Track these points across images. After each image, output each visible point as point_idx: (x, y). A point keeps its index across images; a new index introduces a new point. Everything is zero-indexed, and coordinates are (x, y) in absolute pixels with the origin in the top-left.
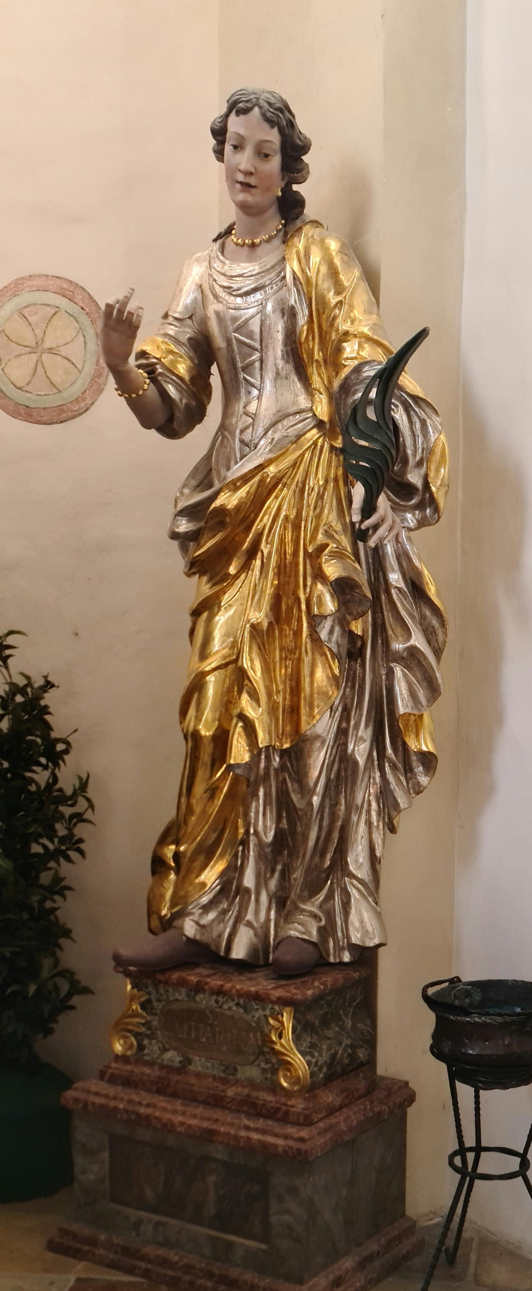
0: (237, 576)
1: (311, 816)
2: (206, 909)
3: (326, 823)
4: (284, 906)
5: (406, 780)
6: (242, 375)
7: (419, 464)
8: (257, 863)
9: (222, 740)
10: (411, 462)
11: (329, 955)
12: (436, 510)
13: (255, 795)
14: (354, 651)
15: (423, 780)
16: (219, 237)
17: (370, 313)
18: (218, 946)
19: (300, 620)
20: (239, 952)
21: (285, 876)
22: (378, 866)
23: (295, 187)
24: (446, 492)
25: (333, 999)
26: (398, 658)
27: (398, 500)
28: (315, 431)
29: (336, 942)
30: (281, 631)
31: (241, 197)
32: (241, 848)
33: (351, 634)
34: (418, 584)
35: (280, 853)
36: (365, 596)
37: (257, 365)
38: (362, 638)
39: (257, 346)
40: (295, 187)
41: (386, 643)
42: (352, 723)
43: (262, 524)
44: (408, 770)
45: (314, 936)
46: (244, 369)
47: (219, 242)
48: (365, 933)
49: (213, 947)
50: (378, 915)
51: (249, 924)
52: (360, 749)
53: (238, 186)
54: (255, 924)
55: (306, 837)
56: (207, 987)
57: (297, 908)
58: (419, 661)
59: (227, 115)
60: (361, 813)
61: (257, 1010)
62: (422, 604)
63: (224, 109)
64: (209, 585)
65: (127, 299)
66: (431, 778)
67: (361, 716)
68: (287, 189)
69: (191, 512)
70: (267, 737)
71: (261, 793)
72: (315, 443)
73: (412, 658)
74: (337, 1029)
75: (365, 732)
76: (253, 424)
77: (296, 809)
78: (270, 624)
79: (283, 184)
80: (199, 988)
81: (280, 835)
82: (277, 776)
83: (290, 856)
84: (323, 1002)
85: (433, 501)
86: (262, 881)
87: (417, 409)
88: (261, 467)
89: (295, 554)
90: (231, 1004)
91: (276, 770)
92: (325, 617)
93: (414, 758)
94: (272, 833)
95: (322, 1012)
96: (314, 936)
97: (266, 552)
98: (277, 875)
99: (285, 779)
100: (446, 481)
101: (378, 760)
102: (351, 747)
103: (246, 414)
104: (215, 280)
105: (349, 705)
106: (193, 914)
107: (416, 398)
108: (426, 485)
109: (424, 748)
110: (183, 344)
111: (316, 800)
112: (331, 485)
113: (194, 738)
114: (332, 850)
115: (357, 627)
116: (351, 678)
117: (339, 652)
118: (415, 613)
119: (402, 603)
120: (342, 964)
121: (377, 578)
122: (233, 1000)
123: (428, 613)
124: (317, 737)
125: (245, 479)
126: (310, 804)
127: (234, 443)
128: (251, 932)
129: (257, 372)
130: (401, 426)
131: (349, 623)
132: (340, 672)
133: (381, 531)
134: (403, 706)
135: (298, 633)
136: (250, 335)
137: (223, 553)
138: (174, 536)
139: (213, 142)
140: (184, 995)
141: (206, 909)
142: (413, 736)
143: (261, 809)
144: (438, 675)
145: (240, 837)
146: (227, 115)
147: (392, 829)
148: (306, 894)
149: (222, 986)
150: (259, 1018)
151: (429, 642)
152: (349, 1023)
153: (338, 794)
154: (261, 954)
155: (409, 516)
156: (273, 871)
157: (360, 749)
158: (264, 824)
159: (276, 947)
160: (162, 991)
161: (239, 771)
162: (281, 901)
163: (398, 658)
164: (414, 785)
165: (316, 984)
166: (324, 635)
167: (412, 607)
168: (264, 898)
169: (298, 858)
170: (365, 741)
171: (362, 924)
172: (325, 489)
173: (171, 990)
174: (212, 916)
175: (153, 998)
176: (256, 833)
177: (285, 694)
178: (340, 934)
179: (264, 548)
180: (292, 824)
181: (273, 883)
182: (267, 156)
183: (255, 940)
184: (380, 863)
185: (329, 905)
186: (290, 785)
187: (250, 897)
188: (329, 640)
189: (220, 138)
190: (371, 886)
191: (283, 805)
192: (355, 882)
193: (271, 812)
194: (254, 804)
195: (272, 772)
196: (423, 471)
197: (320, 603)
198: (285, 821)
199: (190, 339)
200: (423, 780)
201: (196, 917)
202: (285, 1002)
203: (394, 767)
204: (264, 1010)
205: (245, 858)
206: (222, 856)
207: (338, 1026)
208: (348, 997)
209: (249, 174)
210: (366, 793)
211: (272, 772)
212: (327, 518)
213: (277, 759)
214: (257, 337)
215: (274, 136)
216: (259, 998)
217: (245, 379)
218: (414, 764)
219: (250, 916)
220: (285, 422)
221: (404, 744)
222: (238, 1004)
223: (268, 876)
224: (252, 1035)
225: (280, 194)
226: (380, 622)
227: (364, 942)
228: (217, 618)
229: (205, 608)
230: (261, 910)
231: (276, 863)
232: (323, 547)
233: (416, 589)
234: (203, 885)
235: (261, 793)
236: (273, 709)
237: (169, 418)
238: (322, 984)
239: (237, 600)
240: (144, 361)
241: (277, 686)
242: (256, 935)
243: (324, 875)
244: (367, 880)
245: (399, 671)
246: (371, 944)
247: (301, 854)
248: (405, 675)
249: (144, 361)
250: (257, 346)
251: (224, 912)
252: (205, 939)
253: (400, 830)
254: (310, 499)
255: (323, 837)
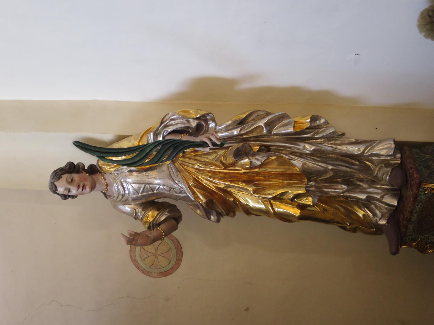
0: (235, 198)
1: (336, 170)
2: (375, 215)
3: (340, 163)
4: (375, 181)
5: (322, 128)
6: (155, 192)
7: (188, 121)
8: (355, 193)
9: (302, 207)
10: (187, 125)
11: (397, 163)
12: (208, 114)
13: (326, 193)
14: (267, 149)
15: (322, 121)
16: (106, 197)
17: (130, 140)
18: (391, 210)
19: (253, 172)
20: (395, 203)
21: (361, 180)
22: (359, 141)
23: (86, 168)
24: (200, 110)
25: (417, 163)
26: (269, 131)
27: (203, 131)
28: (176, 164)
29: (391, 160)
30: (257, 181)
31: (88, 189)
32: (349, 199)
33: (259, 151)
34: (238, 122)
35: (352, 182)
36: (242, 145)
37: (151, 186)
38: (261, 146)
39: (144, 185)
40: (86, 168)
41: (264, 136)
42: (297, 151)
43: (213, 187)
44: (318, 127)
45: (389, 169)
46: (153, 191)
47: (108, 197)
48: (389, 148)
49: (391, 212)
50: (381, 141)
51: (382, 197)
52: (309, 148)
53: (84, 191)
54: (382, 195)
55: (345, 172)
56: (409, 218)
57: (376, 176)
58: (271, 122)
59: (58, 194)
60: (336, 148)
61: (421, 198)
62: (248, 120)
63: (56, 195)
64: (238, 208)
65: (125, 236)
66: (322, 117)
67: (294, 147)
68: (87, 171)
69: (208, 214)
70: (301, 189)
71: (326, 190)
72: (181, 164)
73: (270, 125)
74: (431, 162)
75: (301, 146)
76: (173, 188)
77: (333, 176)
78: (254, 185)
79: (84, 173)
80: (409, 220)
81: (343, 183)
82: (319, 183)
83: (353, 178)
84: (419, 169)
85: (204, 116)
86: (364, 190)
87: (166, 122)
88: (189, 187)
89: (225, 173)
90: (417, 207)
91: (316, 183)
92: (251, 162)
93: (313, 125)
94: (344, 186)
95: (423, 169)
96: (389, 169)
97: (224, 186)
98: (361, 184)
99: (320, 180)
100: (196, 110)
101: (313, 140)
102: (307, 152)
103: (170, 190)
104: (120, 200)
105: (289, 152)
106: (376, 220)
107: (162, 123)
108: (197, 119)
109: (309, 120)
110: (145, 213)
111: (330, 167)
112: (198, 158)
113: (301, 218)
114: (351, 161)
115: (257, 148)
116: (278, 151)
117: (267, 156)
118: (251, 123)
119: (247, 129)
120: (401, 158)
121: (237, 139)
122: (416, 207)
123: (251, 118)
124: (303, 166)
125: (194, 193)
126: (331, 170)
127: (180, 196)
128: (386, 196)
129: (155, 185)
130: (173, 129)
131: (254, 152)
132: (275, 156)
133: (214, 140)
134: (290, 130)
135: (258, 174)
136: (140, 188)
137: (225, 202)
138: (218, 221)
139: (70, 198)
140: (411, 226)
141: (375, 215)
142: (304, 125)
143: (333, 190)
144: (277, 114)
145: (345, 200)
146: (58, 194)
147: (344, 134)
148: (370, 172)
149: (409, 212)
150: (425, 197)
151: (264, 118)
152: (428, 156)
153: (328, 158)
154: (395, 192)
155: (210, 126)
156: (360, 185)
157: (309, 148)
158: (340, 189)
159: (392, 185)
160: (408, 234)
161: (316, 201)
162: (373, 182)
163: (269, 131)
164: (324, 125)
165: (411, 171)
166: (259, 163)
167: (249, 125)
168: (371, 190)
169: (354, 175)
170: (305, 146)
171: (384, 149)
172: (199, 160)
173: (409, 231)
174: (378, 212)
175: (411, 237)
176: (343, 193)
177: (284, 180)
178: (388, 158)
179: (222, 186)
180: (340, 177)
181: (365, 186)
182: (72, 180)
183: (389, 195)
184: (358, 140)
185: (375, 162)
186: (323, 178)
187: (371, 196)
188: (261, 161)
189: (68, 197)
190: (368, 144)
191: (331, 181)
192: (366, 151)
193: (334, 186)
194: (330, 193)
195: (317, 185)
196: (191, 120)
197: (245, 164)
198: (338, 180)
199: (143, 210)
200: (322, 121)
201: (378, 219)
202: (420, 185)
203: (317, 133)
204: (421, 195)
205: (354, 197)
206: (353, 208)
207: (430, 161)
208: (417, 156)
209: (79, 187)
210: (327, 147)
211: (317, 185)
212: (210, 160)
213: (312, 183)
214: (140, 185)
215: (65, 176)
216: (416, 197)
217: (157, 190)
218: (316, 124)
219: (378, 197)
220: (173, 176)
221: (307, 129)
222: (418, 205)
223: (361, 188)
224: (432, 200)
225: (88, 174)
226: (254, 138)
227: (393, 149)
228: (251, 206)
229: (248, 211)
230: (376, 192)
231: (356, 184)
232: (222, 162)
233: (241, 123)
234: (364, 215)
235: (326, 190)
236: (289, 186)
237: (176, 218)
238: (411, 169)
239: (245, 198)
240: (152, 228)
241: (280, 183)
242: (387, 194)
243: (362, 164)
244: (365, 146)
245: (274, 131)
246: (393, 146)
247: (353, 174)
248: (277, 128)
249: (152, 228)
250: (144, 185)
251: (376, 206)
252: (387, 215)
253: (343, 131)
254: (203, 168)
255: (346, 165)
